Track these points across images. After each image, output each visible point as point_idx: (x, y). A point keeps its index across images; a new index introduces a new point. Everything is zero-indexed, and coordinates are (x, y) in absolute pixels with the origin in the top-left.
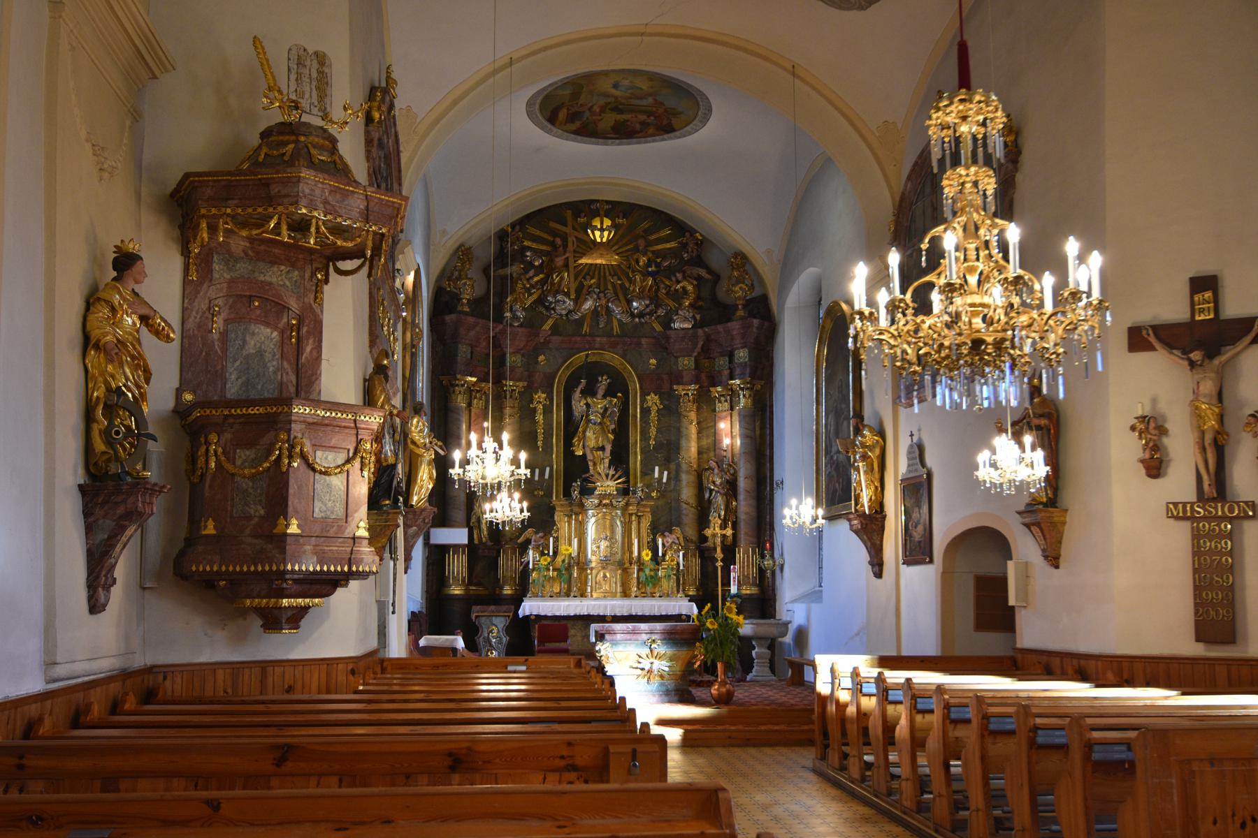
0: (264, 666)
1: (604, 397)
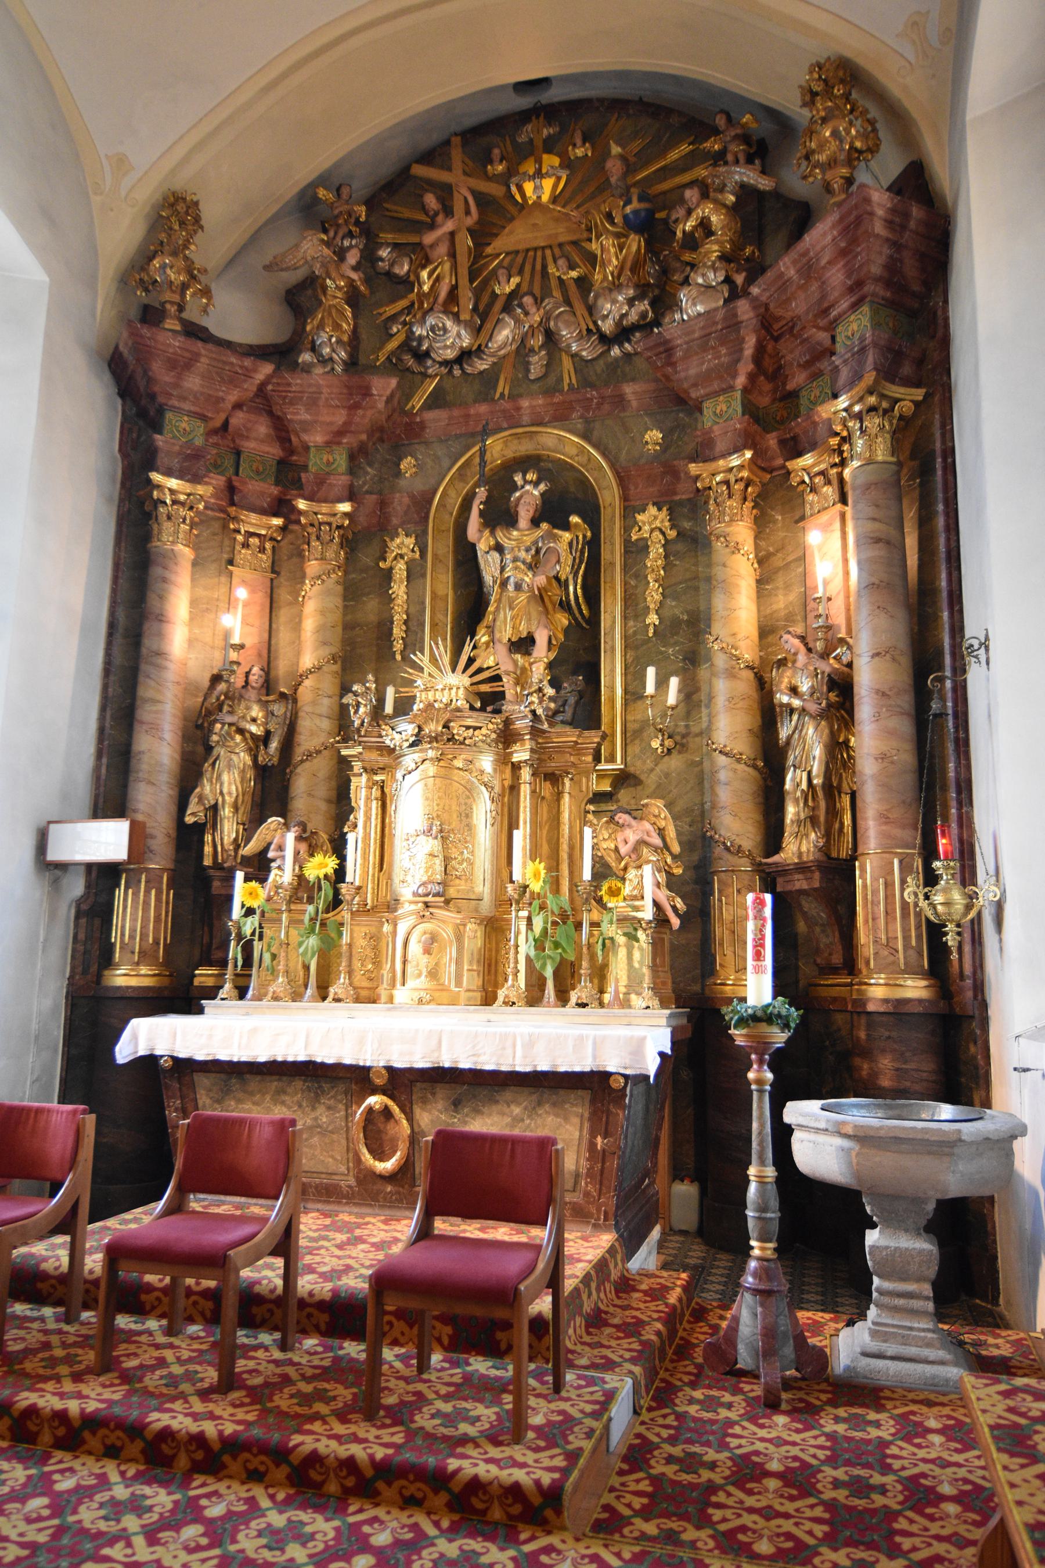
0: (775, 864)
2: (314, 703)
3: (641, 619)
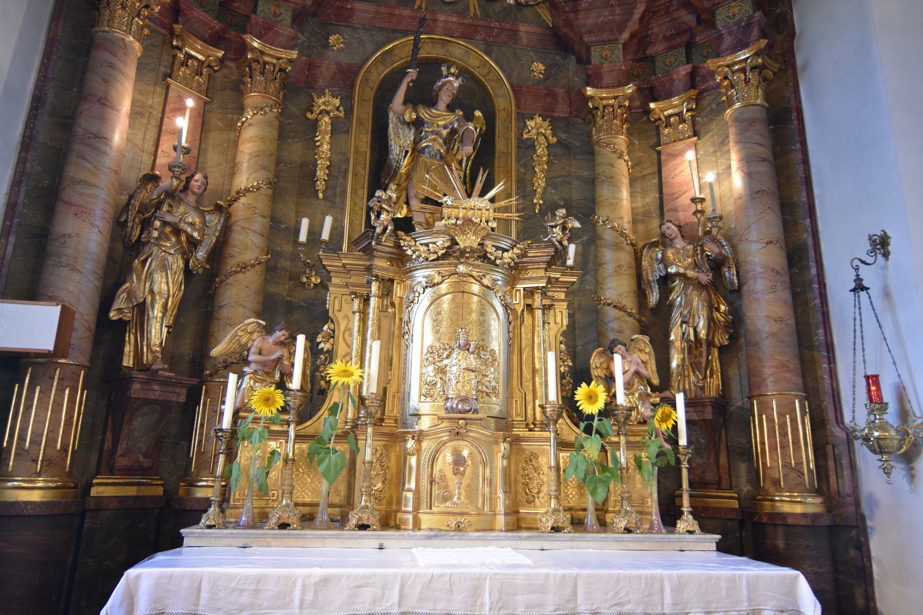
1: (451, 108)
2: (248, 219)
3: (529, 198)
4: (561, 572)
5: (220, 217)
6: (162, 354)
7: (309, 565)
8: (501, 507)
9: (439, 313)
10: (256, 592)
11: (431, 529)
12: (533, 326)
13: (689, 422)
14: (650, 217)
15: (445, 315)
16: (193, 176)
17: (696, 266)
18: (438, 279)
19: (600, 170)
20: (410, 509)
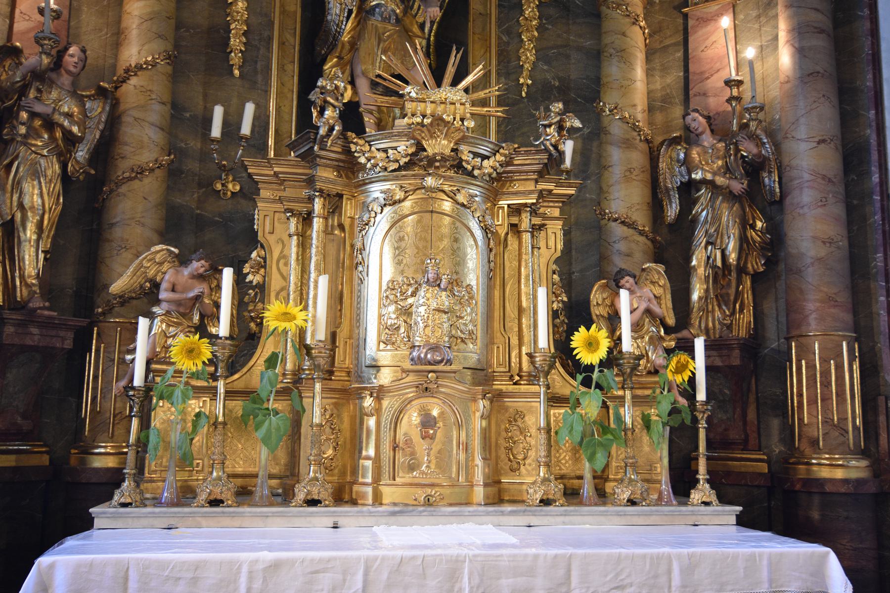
2: (142, 107)
3: (513, 77)
4: (553, 552)
5: (104, 104)
6: (40, 288)
7: (253, 549)
8: (479, 477)
9: (401, 239)
10: (195, 581)
11: (395, 504)
12: (520, 254)
13: (709, 369)
14: (671, 103)
15: (409, 241)
16: (66, 49)
17: (727, 170)
18: (399, 195)
19: (607, 40)
20: (369, 480)
